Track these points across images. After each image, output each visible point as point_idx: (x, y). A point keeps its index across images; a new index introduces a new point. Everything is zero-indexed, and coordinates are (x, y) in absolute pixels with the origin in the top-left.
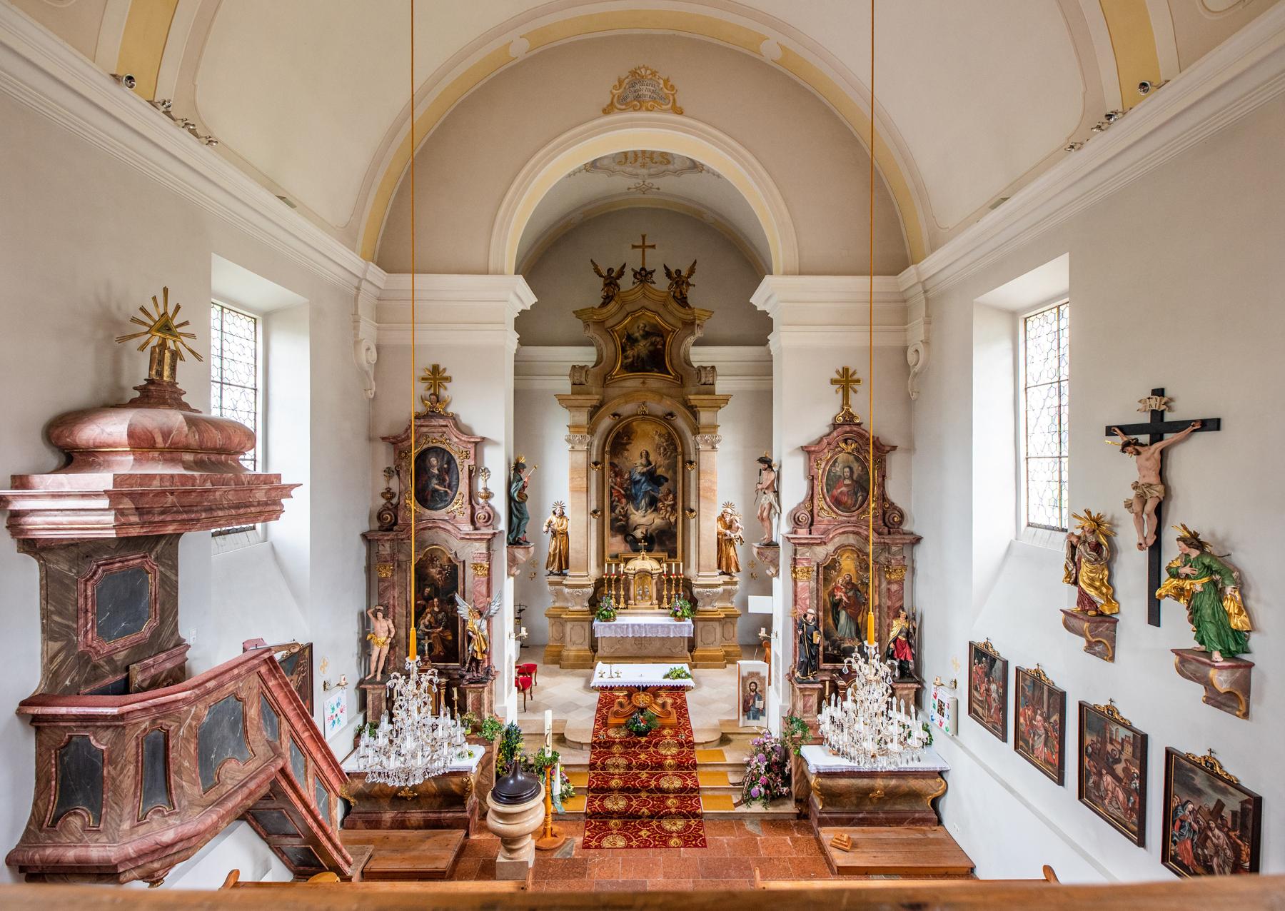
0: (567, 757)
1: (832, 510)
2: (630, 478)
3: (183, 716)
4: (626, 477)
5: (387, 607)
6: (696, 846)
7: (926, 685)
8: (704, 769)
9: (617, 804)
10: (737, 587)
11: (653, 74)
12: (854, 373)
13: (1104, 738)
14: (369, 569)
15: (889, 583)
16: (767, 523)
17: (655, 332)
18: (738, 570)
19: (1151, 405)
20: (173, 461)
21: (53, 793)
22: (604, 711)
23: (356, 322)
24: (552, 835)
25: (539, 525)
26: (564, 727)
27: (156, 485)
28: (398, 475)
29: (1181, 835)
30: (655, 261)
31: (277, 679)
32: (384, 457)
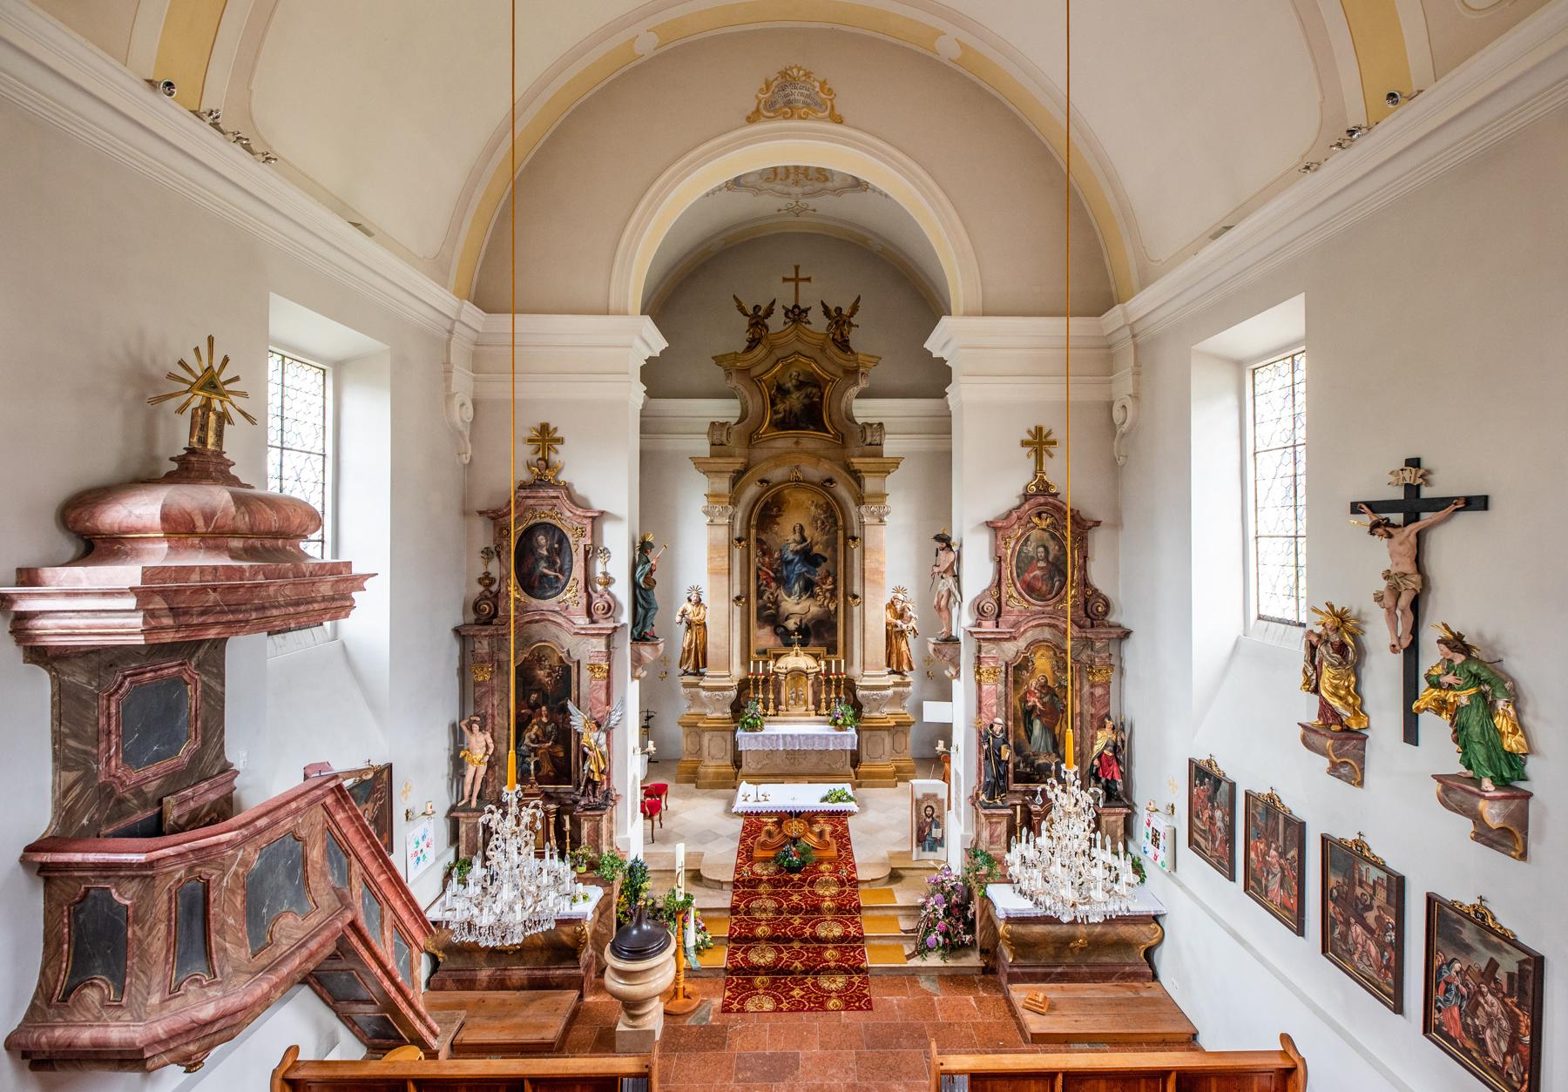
0: (705, 899)
1: (1024, 598)
2: (781, 557)
3: (227, 862)
4: (776, 556)
5: (484, 718)
6: (860, 1008)
7: (1137, 810)
8: (870, 913)
9: (763, 957)
10: (910, 688)
11: (808, 75)
12: (1049, 433)
13: (1352, 880)
14: (462, 671)
15: (1093, 686)
16: (945, 614)
17: (811, 383)
18: (911, 669)
19: (1404, 479)
20: (217, 549)
21: (65, 959)
22: (749, 841)
23: (448, 371)
24: (684, 997)
25: (672, 613)
26: (700, 862)
27: (195, 580)
28: (499, 556)
29: (1447, 1000)
30: (810, 297)
31: (346, 811)
32: (483, 535)
